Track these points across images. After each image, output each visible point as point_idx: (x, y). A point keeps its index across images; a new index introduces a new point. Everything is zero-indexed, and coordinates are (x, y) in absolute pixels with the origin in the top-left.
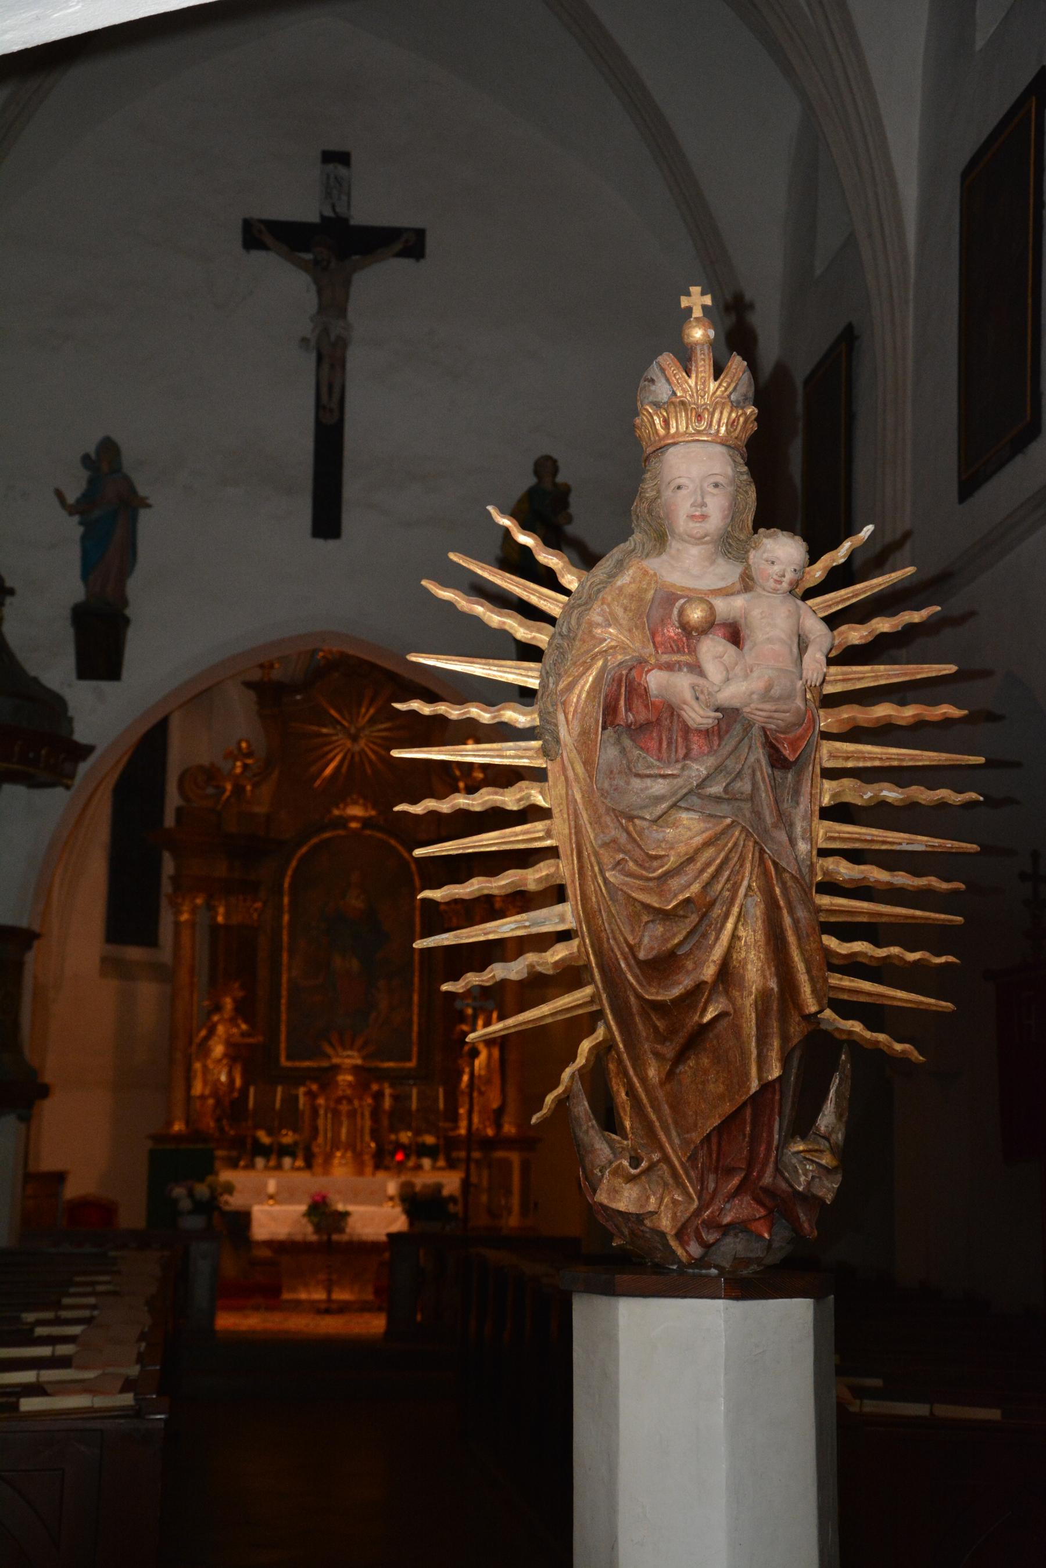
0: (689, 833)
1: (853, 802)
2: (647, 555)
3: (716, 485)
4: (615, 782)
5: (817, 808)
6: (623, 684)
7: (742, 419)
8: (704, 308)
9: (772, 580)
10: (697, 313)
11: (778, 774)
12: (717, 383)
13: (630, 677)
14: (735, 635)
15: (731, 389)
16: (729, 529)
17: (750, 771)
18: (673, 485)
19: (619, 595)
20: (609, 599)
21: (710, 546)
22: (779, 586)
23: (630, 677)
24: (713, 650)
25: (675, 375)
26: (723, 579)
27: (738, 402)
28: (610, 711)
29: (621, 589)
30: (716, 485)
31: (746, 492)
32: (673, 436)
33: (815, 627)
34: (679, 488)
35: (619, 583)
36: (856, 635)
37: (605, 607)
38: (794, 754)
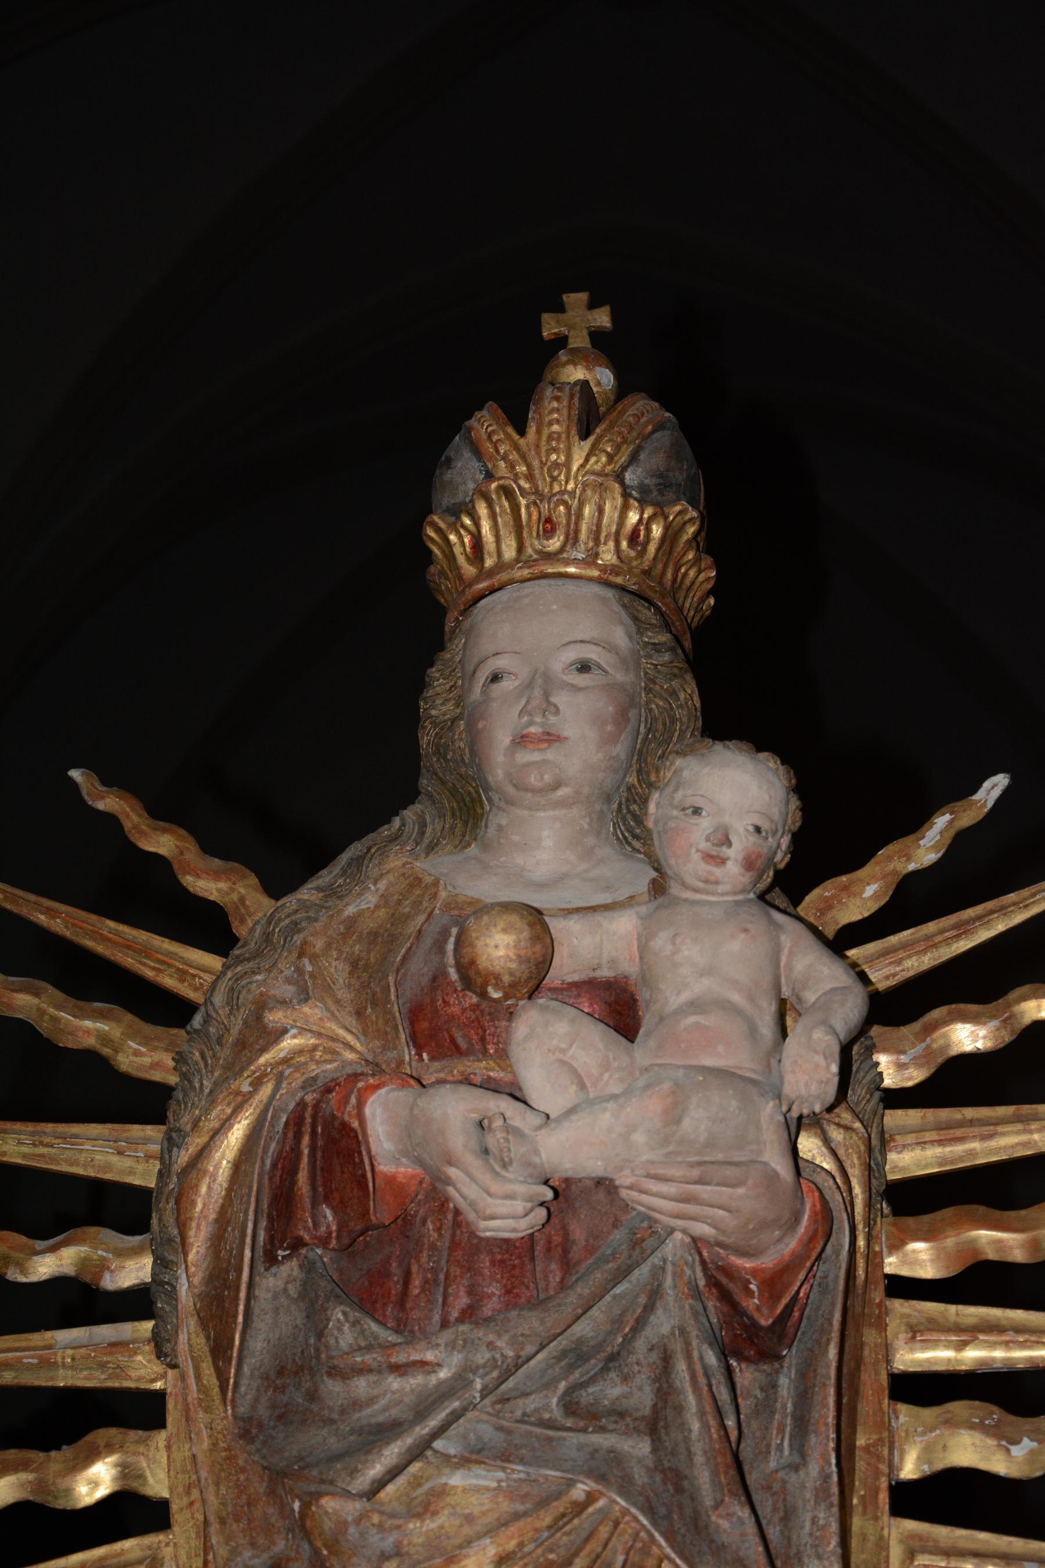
0: (467, 1531)
1: (983, 1466)
2: (431, 848)
3: (584, 667)
4: (285, 1399)
5: (884, 1483)
6: (307, 1129)
7: (657, 531)
8: (597, 337)
9: (696, 857)
10: (579, 340)
11: (746, 1376)
12: (587, 445)
13: (326, 1109)
14: (620, 1009)
15: (623, 459)
16: (632, 779)
17: (654, 1357)
18: (483, 676)
19: (345, 936)
20: (319, 944)
21: (575, 812)
22: (718, 872)
23: (326, 1109)
24: (550, 1046)
25: (489, 436)
26: (607, 889)
27: (644, 489)
28: (282, 1204)
29: (351, 923)
30: (584, 667)
31: (673, 693)
32: (491, 573)
33: (818, 974)
34: (495, 678)
35: (351, 910)
36: (904, 958)
37: (306, 961)
38: (773, 1307)
